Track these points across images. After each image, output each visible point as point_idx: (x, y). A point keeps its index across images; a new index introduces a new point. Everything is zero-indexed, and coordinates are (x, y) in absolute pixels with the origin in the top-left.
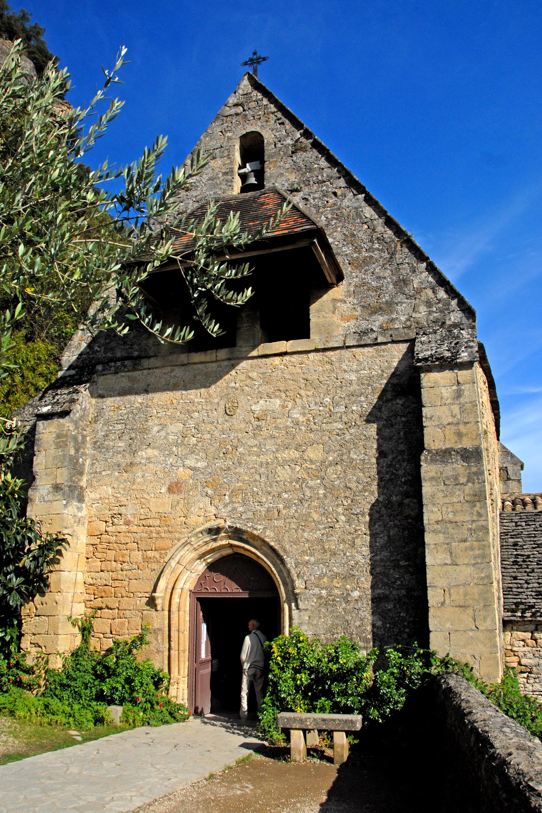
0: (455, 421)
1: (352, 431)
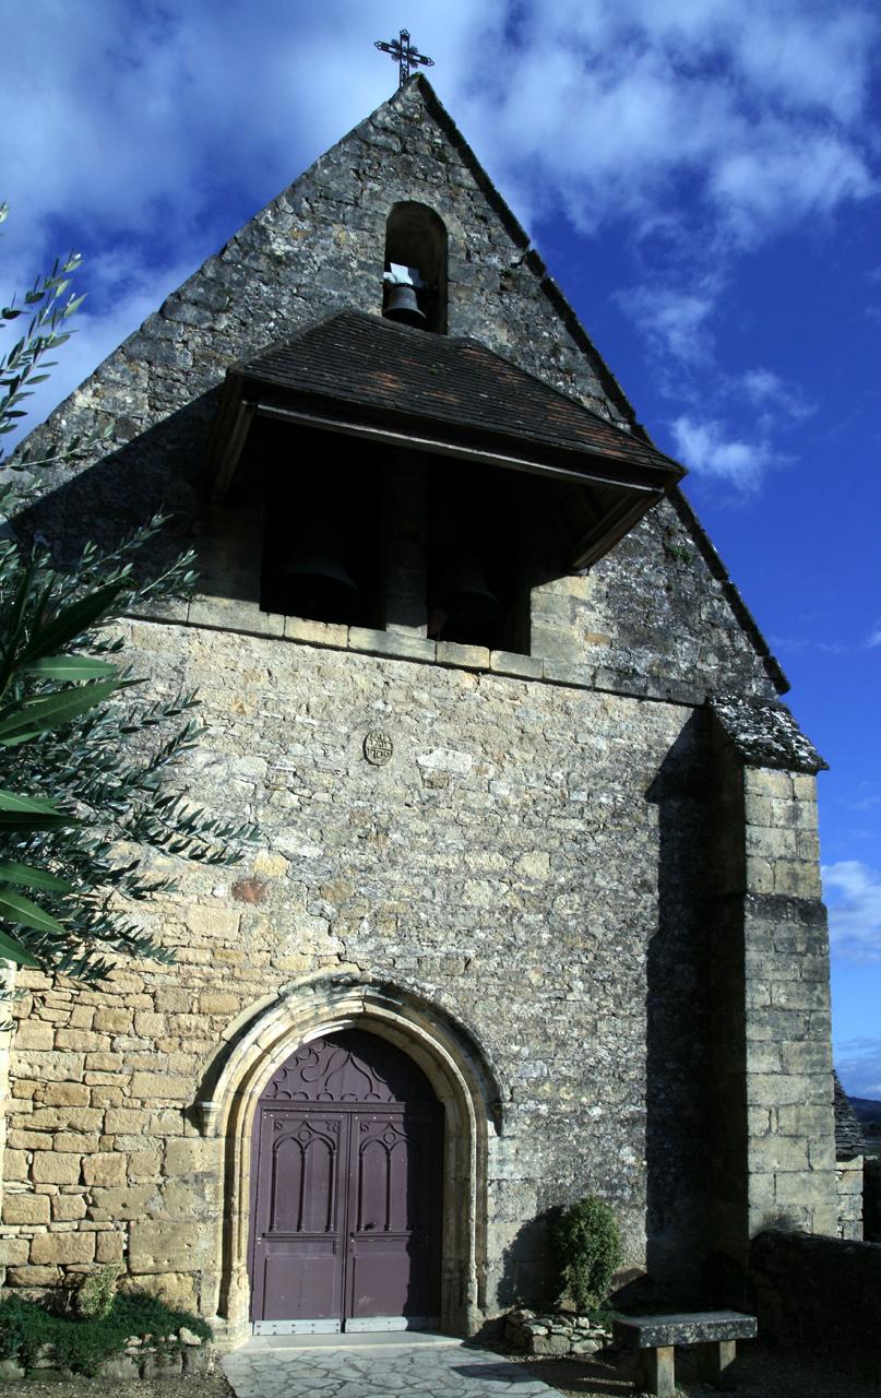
0: (789, 854)
1: (600, 838)
